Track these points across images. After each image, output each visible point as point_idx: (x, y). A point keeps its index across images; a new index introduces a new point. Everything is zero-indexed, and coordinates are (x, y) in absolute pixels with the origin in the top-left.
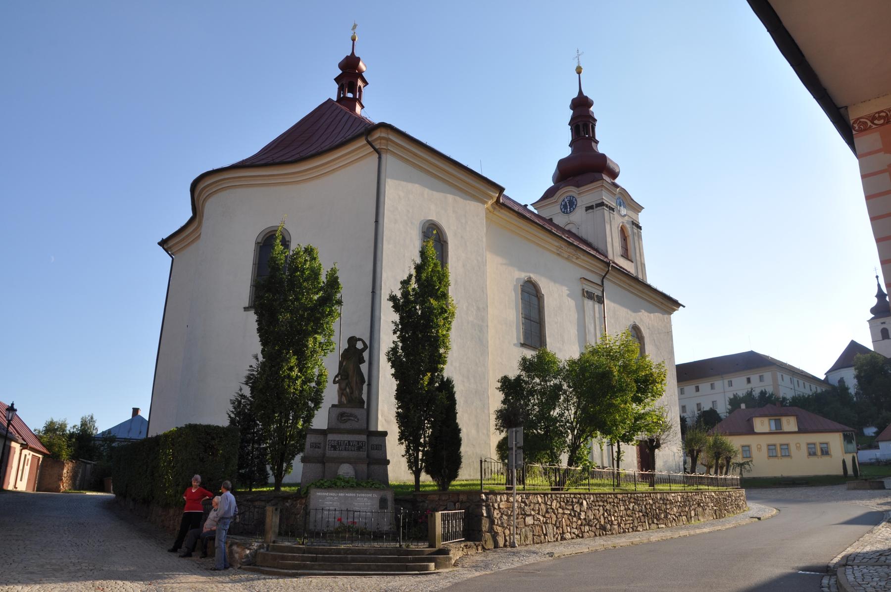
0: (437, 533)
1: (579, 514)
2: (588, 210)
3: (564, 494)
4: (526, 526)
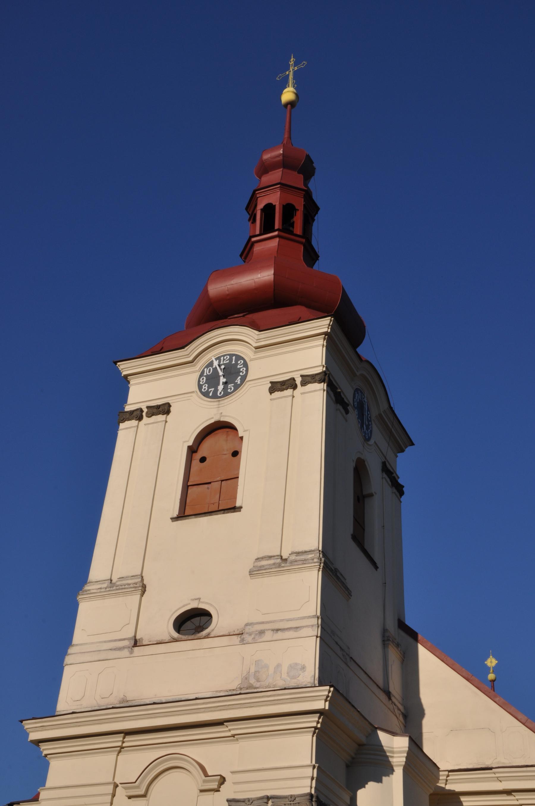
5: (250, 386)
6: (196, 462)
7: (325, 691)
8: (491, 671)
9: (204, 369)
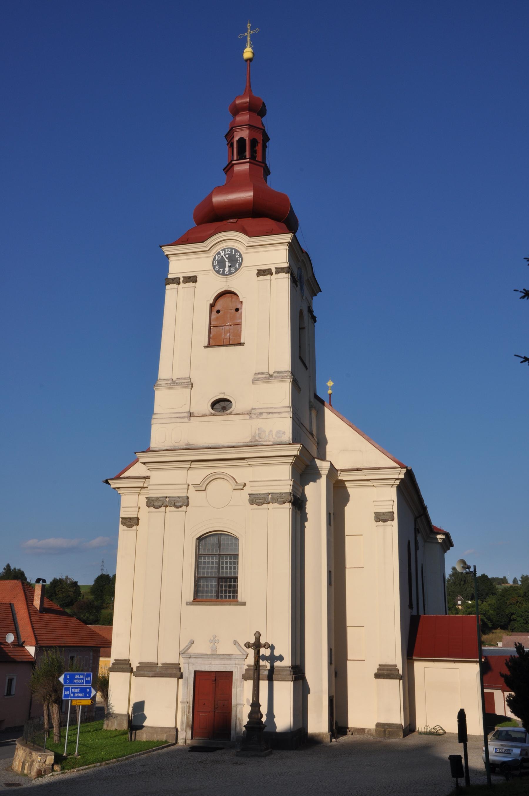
5: (245, 270)
6: (214, 313)
7: (298, 446)
8: (330, 388)
9: (215, 255)
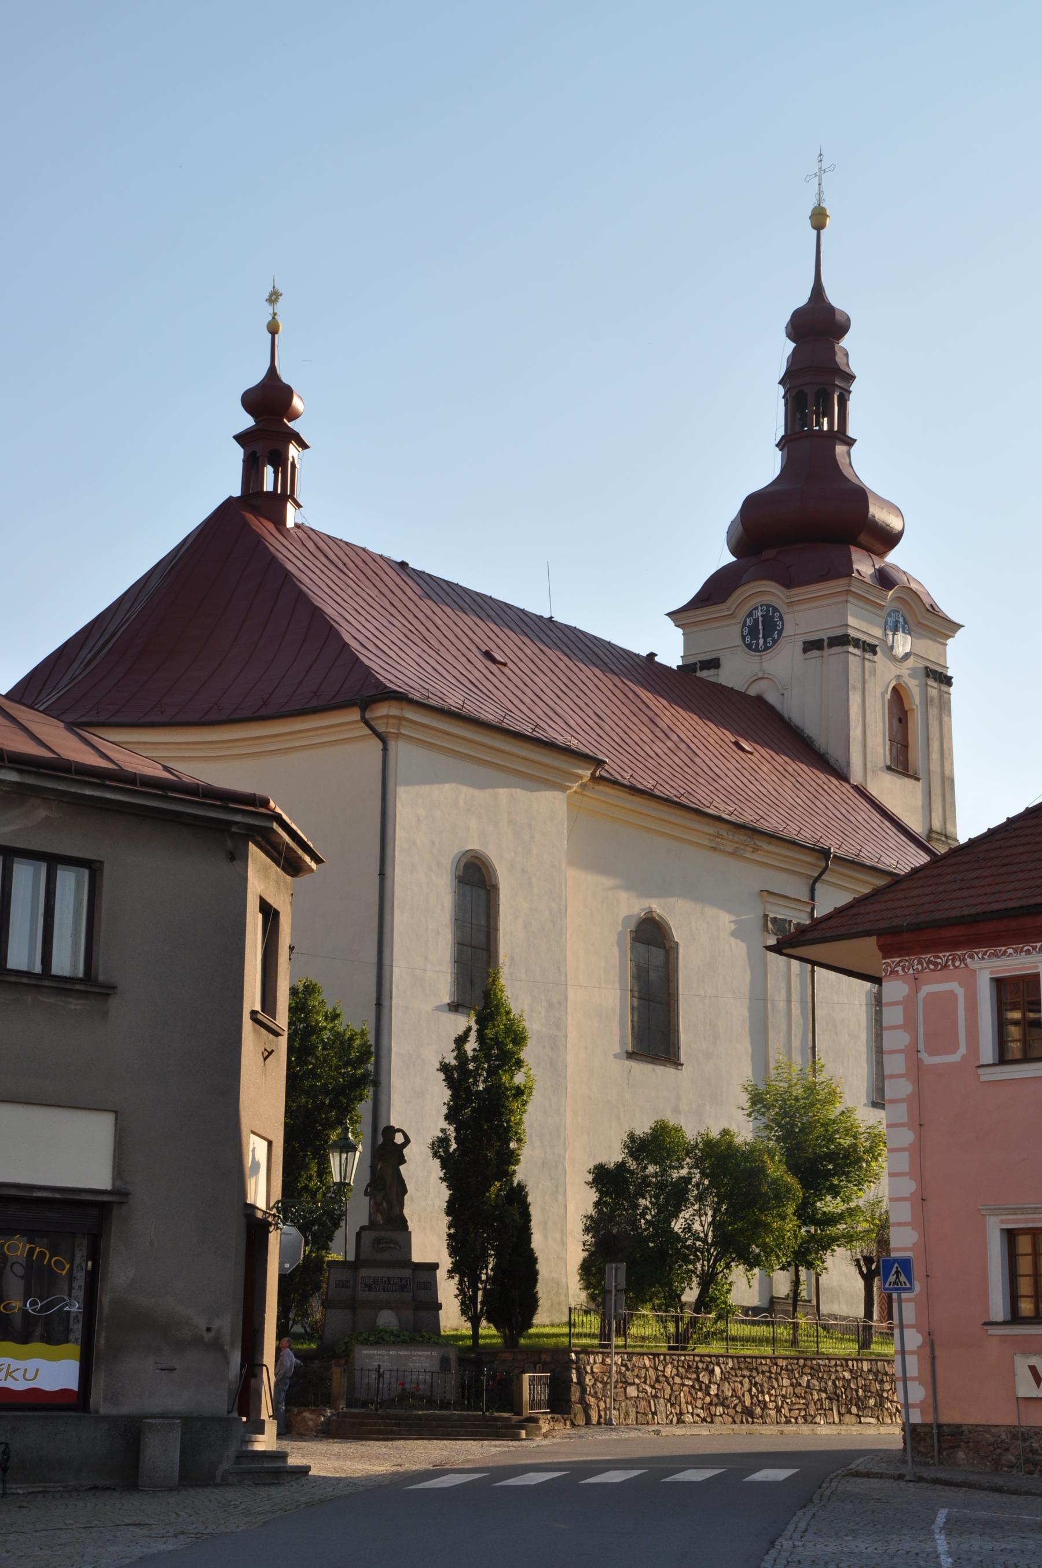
0: (524, 1399)
1: (708, 1387)
2: (810, 650)
3: (685, 1355)
4: (627, 1398)
9: (746, 619)
